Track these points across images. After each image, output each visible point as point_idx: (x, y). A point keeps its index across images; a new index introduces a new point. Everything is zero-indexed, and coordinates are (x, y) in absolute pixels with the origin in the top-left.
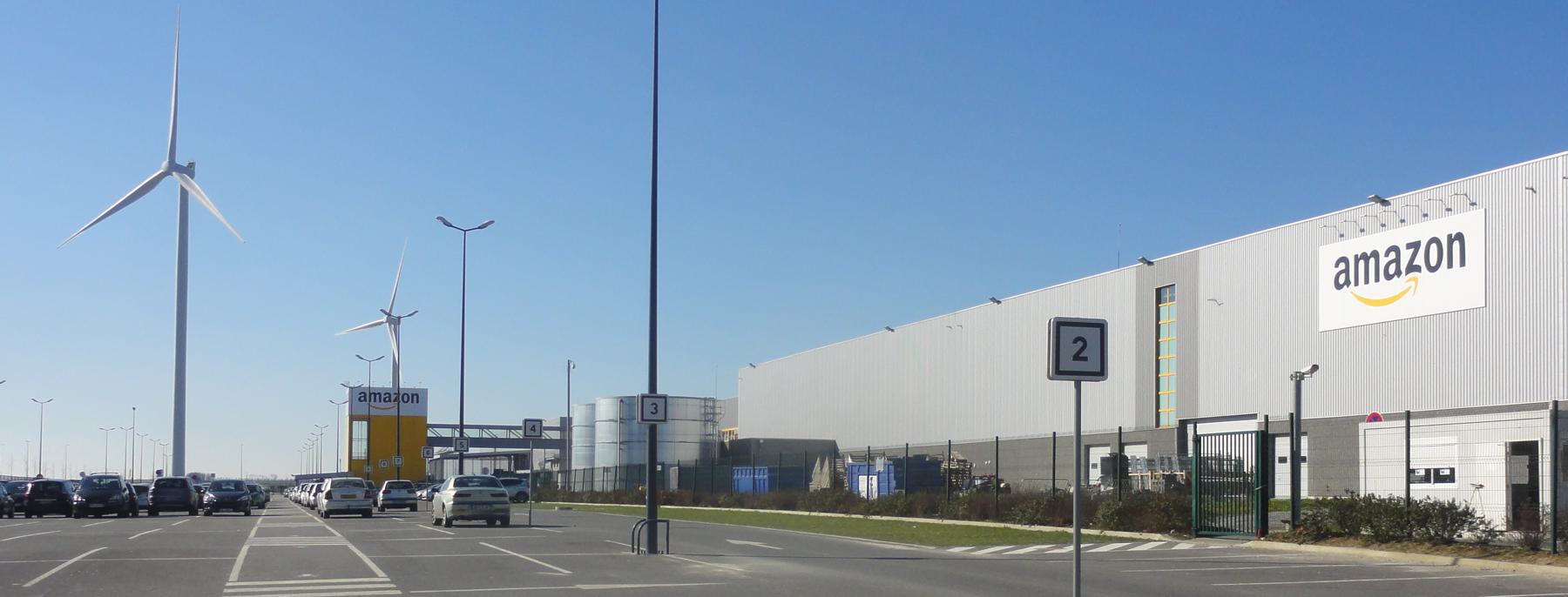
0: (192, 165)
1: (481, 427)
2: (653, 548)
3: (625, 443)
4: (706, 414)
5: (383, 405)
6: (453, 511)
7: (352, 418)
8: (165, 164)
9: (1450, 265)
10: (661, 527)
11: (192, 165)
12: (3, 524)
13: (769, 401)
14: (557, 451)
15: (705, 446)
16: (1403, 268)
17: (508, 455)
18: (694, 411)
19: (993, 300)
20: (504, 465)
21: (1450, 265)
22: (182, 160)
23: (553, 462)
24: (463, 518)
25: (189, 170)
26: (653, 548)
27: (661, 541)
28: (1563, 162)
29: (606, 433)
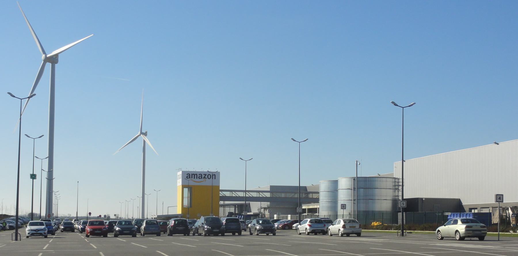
0: (146, 132)
1: (258, 192)
2: (16, 239)
3: (357, 200)
4: (395, 186)
5: (198, 180)
6: (310, 230)
7: (183, 187)
8: (139, 133)
10: (19, 235)
11: (146, 132)
12: (517, 195)
13: (425, 179)
14: (269, 203)
15: (395, 202)
17: (235, 205)
18: (390, 184)
19: (496, 143)
20: (232, 210)
22: (144, 131)
23: (265, 209)
24: (469, 237)
25: (145, 134)
26: (16, 239)
27: (19, 238)
28: (1, 214)
29: (344, 196)
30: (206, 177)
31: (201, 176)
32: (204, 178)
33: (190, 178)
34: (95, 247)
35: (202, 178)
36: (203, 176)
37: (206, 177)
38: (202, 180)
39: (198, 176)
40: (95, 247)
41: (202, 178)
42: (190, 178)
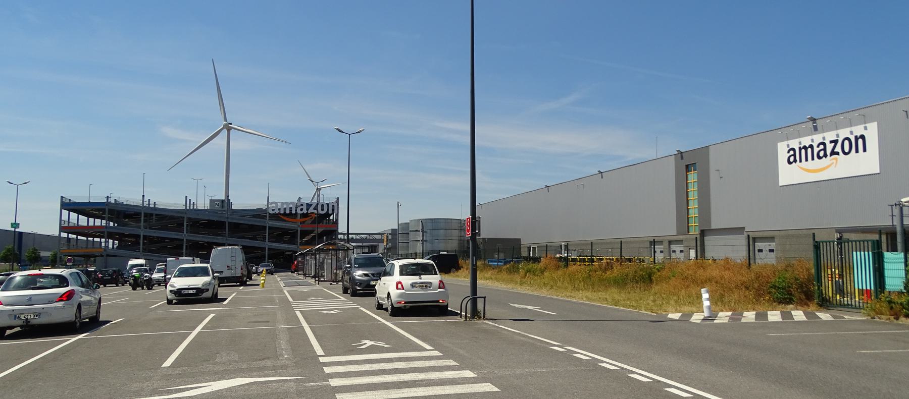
9: (857, 151)
16: (828, 152)
21: (857, 151)
30: (838, 149)
31: (825, 149)
32: (833, 153)
33: (795, 161)
34: (168, 363)
35: (825, 155)
39: (816, 150)
40: (168, 363)
41: (825, 155)
42: (795, 161)
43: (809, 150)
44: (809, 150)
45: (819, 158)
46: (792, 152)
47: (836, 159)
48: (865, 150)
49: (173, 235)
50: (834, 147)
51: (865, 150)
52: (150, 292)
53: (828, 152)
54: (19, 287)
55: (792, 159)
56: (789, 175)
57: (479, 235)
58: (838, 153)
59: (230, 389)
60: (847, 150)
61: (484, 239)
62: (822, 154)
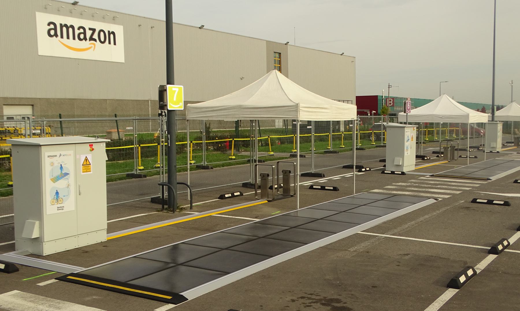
16: (88, 37)
30: (95, 36)
31: (85, 33)
32: (91, 39)
33: (56, 35)
35: (85, 39)
36: (89, 33)
37: (95, 36)
38: (86, 44)
39: (77, 32)
41: (85, 39)
42: (56, 35)
43: (71, 30)
44: (71, 30)
45: (80, 39)
46: (52, 26)
47: (94, 44)
48: (115, 44)
49: (331, 129)
50: (93, 34)
51: (115, 44)
52: (325, 296)
53: (88, 37)
54: (514, 130)
55: (52, 32)
56: (49, 47)
57: (489, 116)
58: (95, 40)
59: (384, 223)
60: (102, 40)
61: (359, 113)
62: (82, 36)
